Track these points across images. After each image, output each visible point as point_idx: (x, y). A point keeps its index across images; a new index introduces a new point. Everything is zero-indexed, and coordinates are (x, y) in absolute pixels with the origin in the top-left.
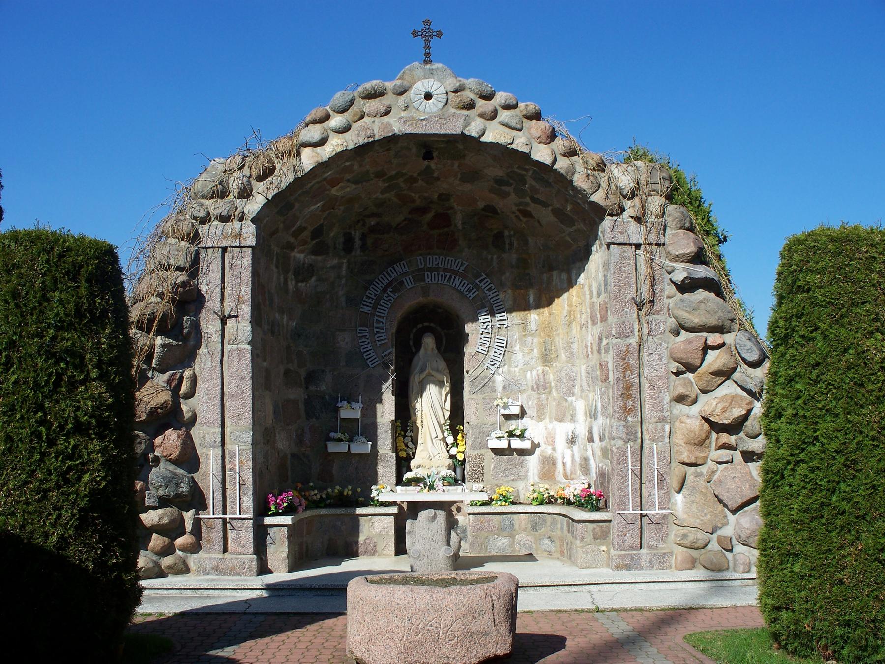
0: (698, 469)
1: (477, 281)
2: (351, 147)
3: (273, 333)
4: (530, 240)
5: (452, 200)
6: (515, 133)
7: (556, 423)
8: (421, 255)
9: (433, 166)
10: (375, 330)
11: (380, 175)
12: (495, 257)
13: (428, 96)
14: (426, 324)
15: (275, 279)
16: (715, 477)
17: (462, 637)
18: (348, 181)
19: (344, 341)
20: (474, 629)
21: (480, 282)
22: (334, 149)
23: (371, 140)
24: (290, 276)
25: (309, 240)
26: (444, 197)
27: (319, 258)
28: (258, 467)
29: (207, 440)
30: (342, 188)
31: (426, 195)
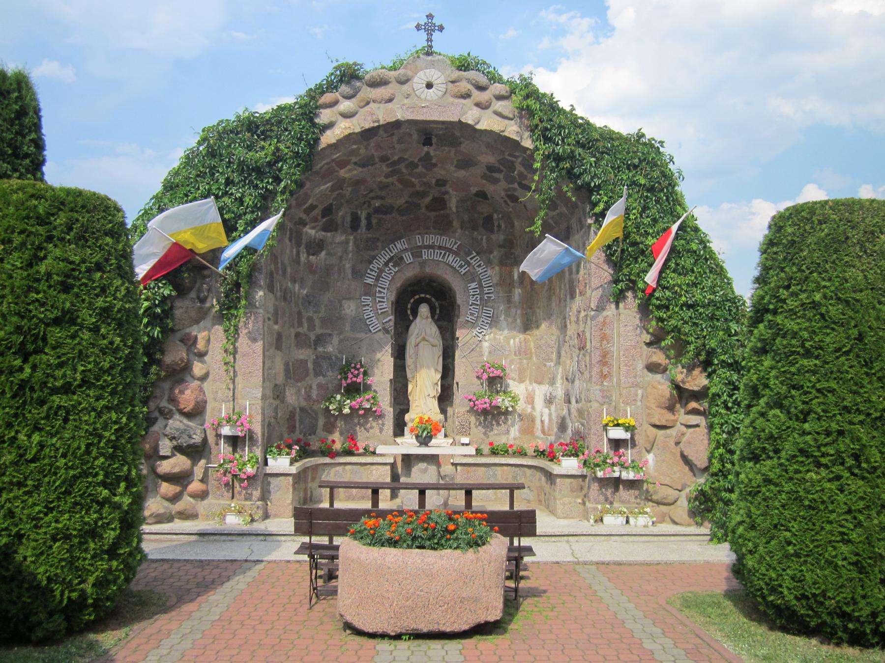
0: (668, 431)
1: (468, 259)
2: (358, 130)
3: (285, 299)
4: (516, 223)
5: (448, 185)
6: (507, 122)
7: (534, 385)
8: (419, 234)
9: (432, 153)
10: (378, 299)
11: (384, 159)
12: (484, 237)
13: (429, 86)
14: (423, 295)
15: (288, 251)
16: (684, 439)
17: (452, 603)
18: (355, 163)
19: (350, 308)
20: (464, 595)
21: (471, 259)
22: (342, 132)
23: (376, 124)
24: (303, 249)
25: (319, 217)
26: (441, 183)
27: (329, 234)
28: (267, 421)
29: (220, 395)
30: (350, 170)
31: (425, 180)
